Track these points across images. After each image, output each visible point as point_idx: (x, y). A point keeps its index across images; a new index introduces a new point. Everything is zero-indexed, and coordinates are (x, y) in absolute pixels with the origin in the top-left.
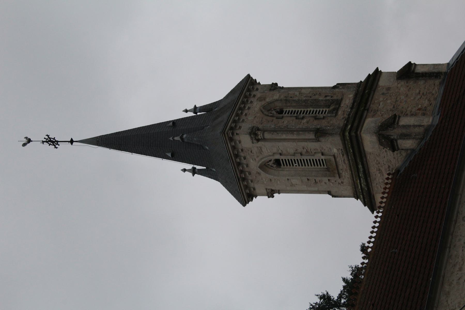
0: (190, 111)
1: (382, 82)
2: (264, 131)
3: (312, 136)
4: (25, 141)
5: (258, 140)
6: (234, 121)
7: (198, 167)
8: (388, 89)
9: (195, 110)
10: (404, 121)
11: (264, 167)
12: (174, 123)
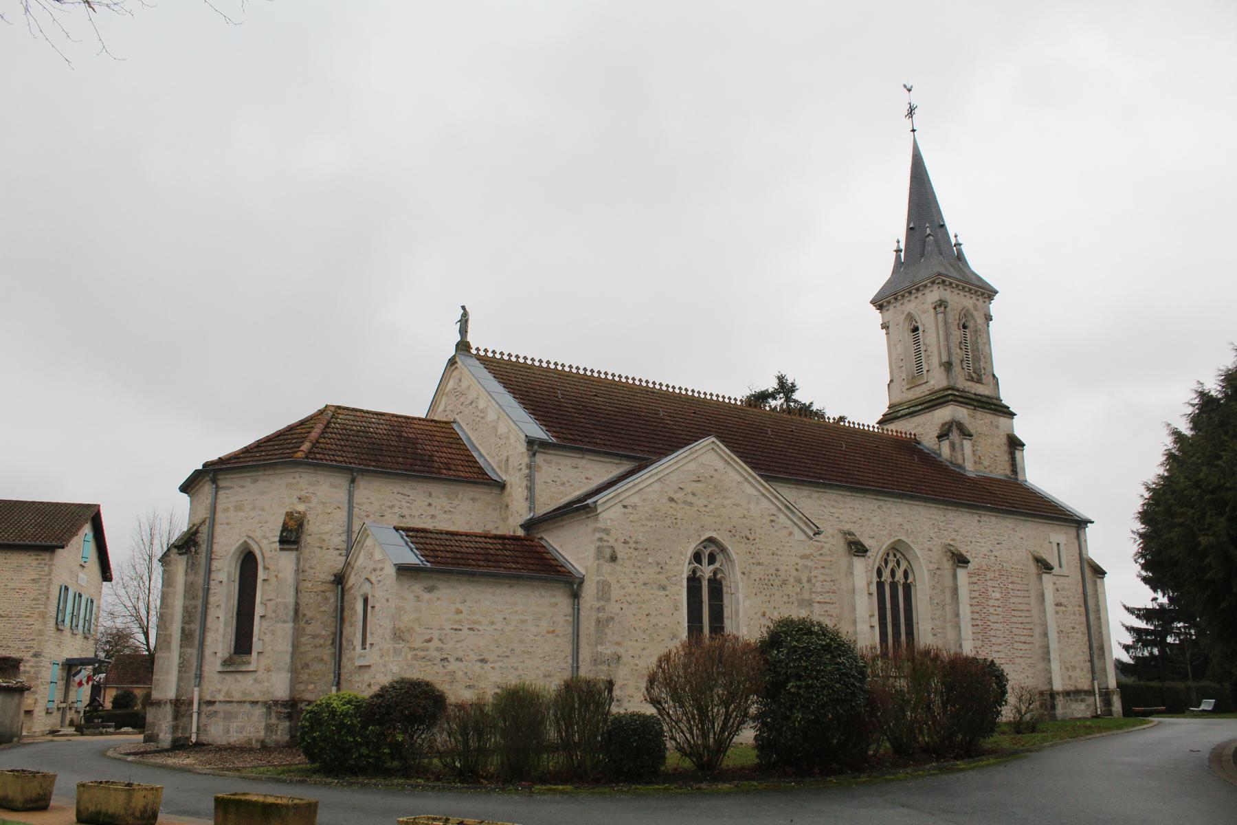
1: (1003, 421)
3: (945, 359)
4: (909, 87)
5: (935, 308)
6: (951, 284)
7: (902, 254)
8: (997, 427)
11: (910, 317)
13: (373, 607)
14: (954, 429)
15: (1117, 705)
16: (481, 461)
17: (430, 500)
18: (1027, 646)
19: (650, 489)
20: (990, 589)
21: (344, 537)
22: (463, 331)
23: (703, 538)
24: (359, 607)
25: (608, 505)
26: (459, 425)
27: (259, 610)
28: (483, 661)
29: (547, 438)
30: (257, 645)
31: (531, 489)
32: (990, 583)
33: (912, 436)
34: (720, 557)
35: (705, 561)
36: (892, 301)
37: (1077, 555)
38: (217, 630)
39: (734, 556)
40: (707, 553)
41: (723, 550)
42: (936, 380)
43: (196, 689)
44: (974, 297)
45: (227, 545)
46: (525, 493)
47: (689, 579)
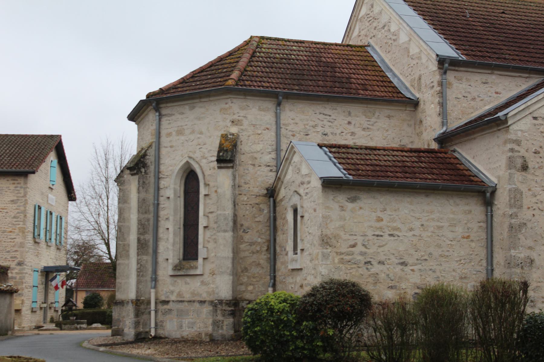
13: (302, 217)
17: (349, 119)
21: (273, 155)
25: (518, 117)
26: (373, 48)
27: (202, 222)
28: (404, 264)
30: (202, 252)
31: (442, 105)
43: (153, 291)
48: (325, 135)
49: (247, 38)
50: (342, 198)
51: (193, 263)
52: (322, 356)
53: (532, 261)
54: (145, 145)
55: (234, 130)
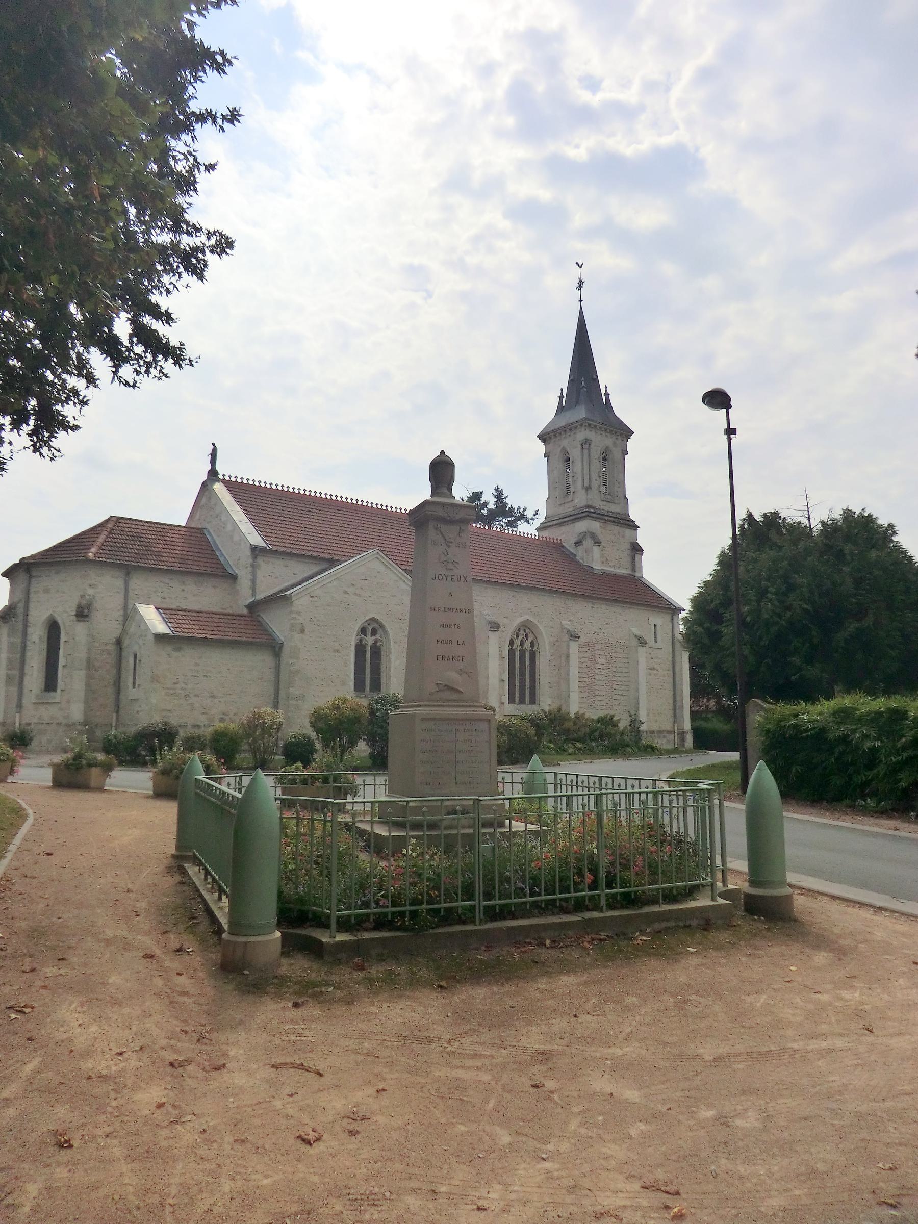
0: (606, 391)
1: (628, 532)
2: (589, 449)
3: (586, 484)
4: (580, 264)
5: (582, 445)
6: (595, 426)
7: (564, 400)
8: (623, 536)
9: (607, 394)
10: (596, 549)
11: (565, 451)
12: (596, 380)
13: (140, 661)
14: (588, 536)
15: (689, 741)
16: (222, 559)
17: (183, 587)
18: (623, 698)
19: (330, 585)
20: (597, 657)
21: (122, 612)
22: (213, 461)
23: (367, 618)
24: (131, 661)
25: (299, 596)
26: (209, 532)
27: (62, 661)
28: (213, 697)
29: (265, 545)
30: (60, 684)
31: (253, 582)
32: (597, 652)
33: (559, 541)
34: (380, 632)
35: (369, 633)
36: (553, 437)
37: (670, 634)
38: (32, 675)
39: (390, 631)
40: (370, 629)
41: (382, 626)
42: (580, 499)
43: (18, 715)
44: (614, 437)
45: (39, 616)
46: (250, 583)
47: (357, 646)
48: (164, 598)
49: (106, 518)
50: (169, 648)
51: (53, 694)
52: (804, 589)
53: (304, 696)
54: (16, 600)
55: (90, 591)
